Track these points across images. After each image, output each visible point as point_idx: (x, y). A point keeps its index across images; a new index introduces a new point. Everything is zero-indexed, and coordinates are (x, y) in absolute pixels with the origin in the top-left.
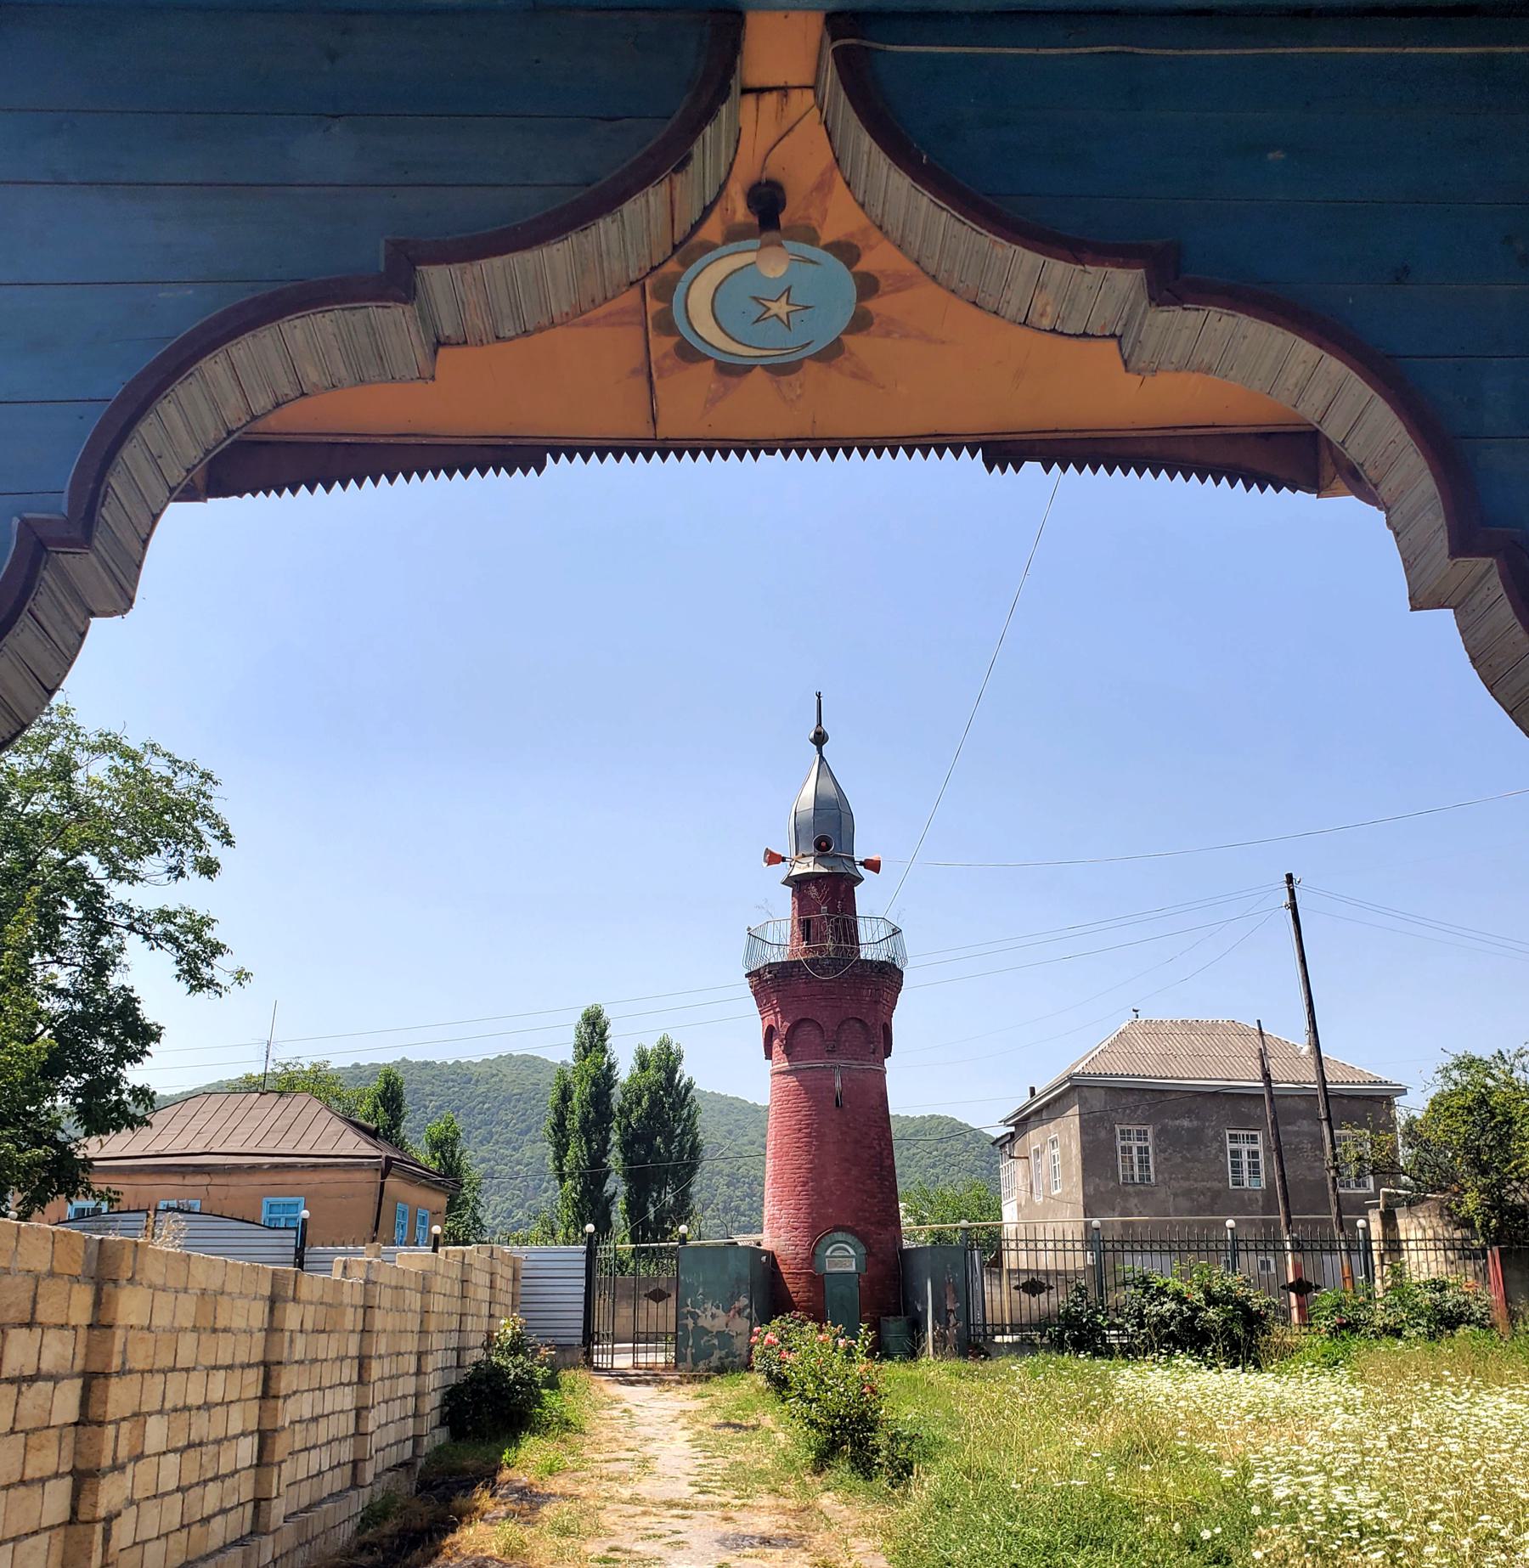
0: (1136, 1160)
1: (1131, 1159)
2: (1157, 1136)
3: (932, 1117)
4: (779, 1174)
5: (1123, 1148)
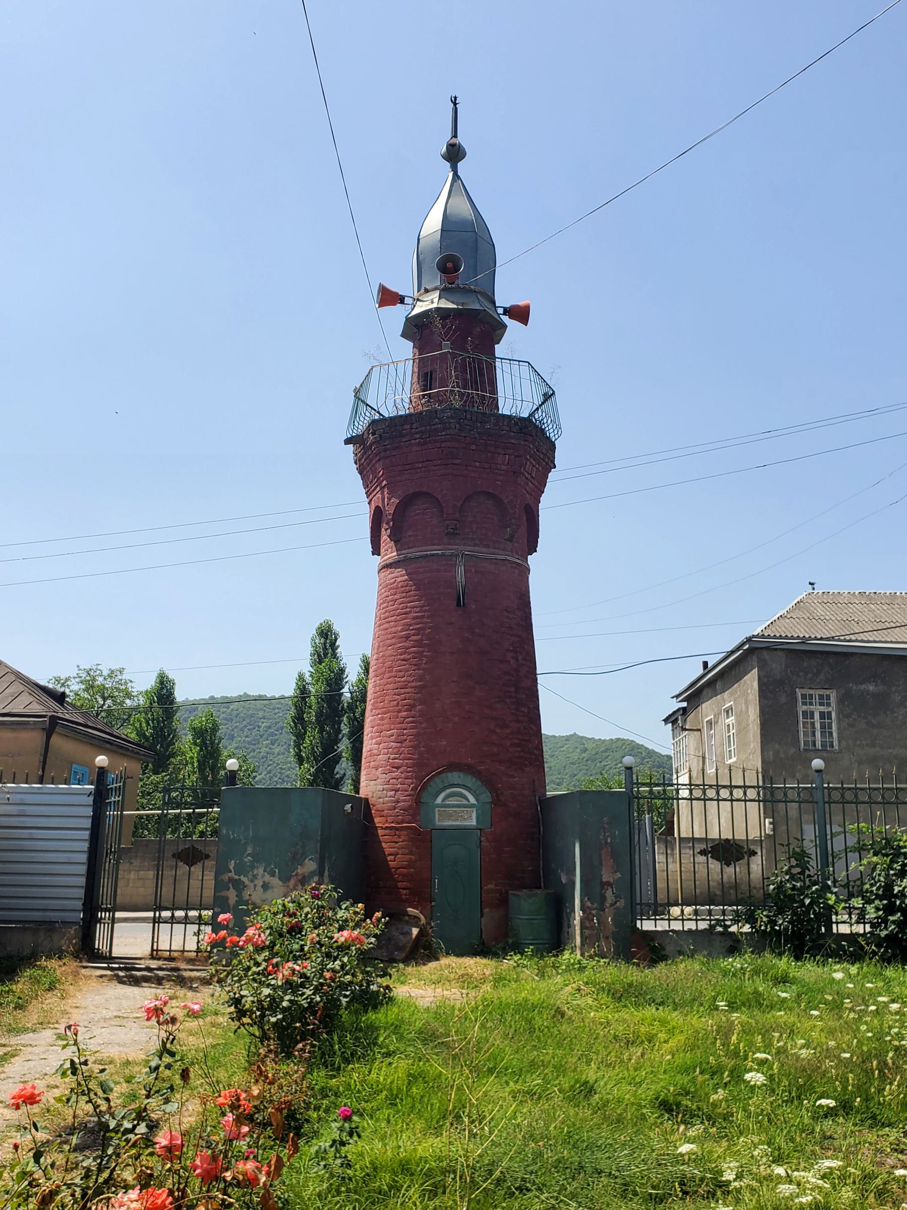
0: (818, 726)
1: (813, 724)
2: (840, 701)
3: (618, 739)
4: (381, 694)
5: (805, 713)
